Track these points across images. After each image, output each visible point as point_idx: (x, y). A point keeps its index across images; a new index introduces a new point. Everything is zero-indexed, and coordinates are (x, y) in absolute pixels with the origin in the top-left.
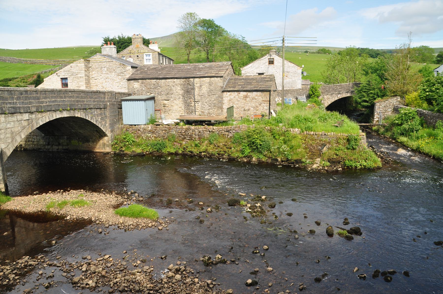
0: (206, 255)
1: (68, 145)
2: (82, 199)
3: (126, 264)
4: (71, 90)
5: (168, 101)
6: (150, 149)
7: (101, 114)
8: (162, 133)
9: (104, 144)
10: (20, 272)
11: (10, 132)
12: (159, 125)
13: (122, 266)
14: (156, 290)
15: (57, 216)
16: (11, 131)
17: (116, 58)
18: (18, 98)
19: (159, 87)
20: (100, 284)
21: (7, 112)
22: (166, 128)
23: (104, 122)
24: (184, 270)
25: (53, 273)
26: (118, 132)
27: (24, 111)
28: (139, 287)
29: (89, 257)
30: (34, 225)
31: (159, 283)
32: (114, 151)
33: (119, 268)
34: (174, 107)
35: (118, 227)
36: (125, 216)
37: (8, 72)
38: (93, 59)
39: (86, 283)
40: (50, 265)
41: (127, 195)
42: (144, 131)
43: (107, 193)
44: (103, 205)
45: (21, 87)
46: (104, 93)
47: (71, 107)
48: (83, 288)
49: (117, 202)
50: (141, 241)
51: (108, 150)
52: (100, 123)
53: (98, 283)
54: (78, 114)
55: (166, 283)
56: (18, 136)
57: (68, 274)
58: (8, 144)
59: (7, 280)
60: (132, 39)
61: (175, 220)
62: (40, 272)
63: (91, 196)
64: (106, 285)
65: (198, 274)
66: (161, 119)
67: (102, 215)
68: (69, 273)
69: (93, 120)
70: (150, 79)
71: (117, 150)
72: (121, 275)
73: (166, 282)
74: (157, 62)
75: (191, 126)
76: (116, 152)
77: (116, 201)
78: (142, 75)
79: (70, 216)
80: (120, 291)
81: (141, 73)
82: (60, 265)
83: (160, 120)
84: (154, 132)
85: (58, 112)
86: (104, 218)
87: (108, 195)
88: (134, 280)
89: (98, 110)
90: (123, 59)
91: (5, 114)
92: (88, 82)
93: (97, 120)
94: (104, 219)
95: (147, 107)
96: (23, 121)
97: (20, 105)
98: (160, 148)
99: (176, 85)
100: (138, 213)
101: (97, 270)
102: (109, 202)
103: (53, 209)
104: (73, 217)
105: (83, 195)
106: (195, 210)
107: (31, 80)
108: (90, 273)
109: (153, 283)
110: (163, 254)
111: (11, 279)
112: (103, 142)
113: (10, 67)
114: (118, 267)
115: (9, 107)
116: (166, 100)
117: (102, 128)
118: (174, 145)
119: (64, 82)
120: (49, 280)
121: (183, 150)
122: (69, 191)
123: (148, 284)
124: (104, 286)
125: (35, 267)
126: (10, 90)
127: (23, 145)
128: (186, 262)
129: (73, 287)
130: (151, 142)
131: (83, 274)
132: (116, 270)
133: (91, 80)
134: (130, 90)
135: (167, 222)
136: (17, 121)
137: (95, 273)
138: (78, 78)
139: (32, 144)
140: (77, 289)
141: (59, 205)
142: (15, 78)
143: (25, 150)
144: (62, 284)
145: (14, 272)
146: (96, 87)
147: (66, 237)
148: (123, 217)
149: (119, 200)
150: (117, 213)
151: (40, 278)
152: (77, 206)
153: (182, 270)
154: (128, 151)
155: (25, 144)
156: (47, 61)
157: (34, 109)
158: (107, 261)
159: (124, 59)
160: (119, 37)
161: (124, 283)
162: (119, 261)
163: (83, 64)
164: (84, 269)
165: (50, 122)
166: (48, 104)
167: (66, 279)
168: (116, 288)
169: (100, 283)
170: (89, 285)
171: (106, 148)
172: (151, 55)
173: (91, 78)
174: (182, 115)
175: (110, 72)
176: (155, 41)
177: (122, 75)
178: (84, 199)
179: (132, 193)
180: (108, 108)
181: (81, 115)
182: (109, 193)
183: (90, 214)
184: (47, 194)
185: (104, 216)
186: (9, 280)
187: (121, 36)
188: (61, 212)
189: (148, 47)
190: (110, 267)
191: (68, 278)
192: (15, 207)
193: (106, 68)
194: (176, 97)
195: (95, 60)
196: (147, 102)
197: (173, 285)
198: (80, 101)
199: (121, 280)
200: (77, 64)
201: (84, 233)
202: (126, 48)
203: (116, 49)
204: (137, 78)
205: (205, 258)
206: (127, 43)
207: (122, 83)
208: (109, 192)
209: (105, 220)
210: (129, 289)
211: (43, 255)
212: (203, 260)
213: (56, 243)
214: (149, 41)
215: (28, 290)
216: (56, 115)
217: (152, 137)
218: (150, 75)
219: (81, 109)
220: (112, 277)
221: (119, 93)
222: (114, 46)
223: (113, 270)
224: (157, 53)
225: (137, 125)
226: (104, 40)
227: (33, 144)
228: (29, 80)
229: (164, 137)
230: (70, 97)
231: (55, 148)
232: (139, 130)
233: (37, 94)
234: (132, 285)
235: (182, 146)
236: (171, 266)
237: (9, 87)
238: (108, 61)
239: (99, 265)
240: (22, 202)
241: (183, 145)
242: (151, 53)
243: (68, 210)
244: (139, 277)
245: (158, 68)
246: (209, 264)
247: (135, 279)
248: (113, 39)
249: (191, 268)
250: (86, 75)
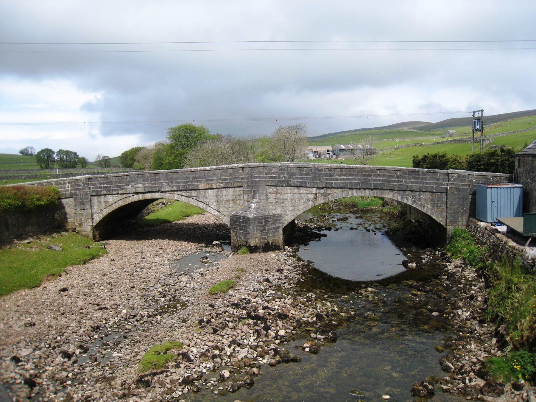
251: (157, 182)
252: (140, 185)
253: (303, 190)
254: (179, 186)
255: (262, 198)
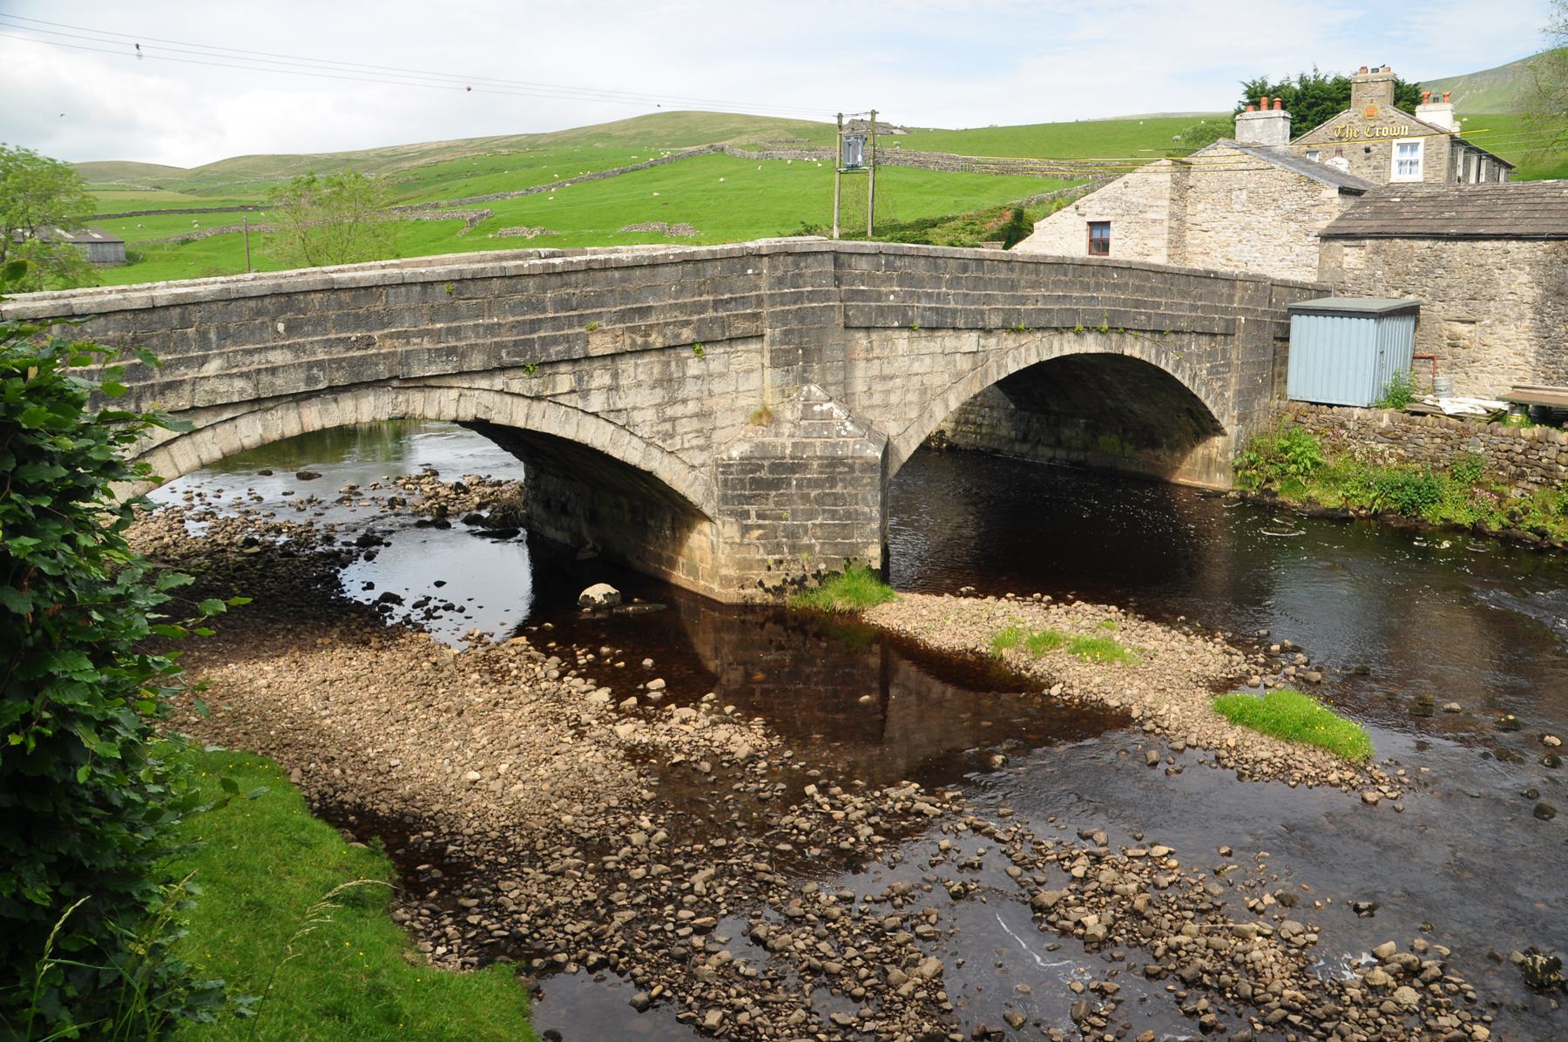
0: (1542, 947)
1: (1085, 449)
2: (1111, 638)
3: (1221, 894)
4: (1121, 262)
5: (1472, 327)
6: (1375, 499)
7: (1211, 355)
8: (1429, 446)
9: (1209, 462)
10: (888, 826)
11: (918, 386)
12: (1424, 414)
13: (1208, 897)
14: (1315, 1017)
15: (1020, 676)
16: (922, 384)
17: (1286, 154)
18: (955, 282)
19: (1440, 271)
20: (1121, 935)
21: (918, 323)
22: (1448, 426)
23: (1220, 383)
24: (1436, 979)
25: (980, 855)
26: (1263, 423)
27: (966, 322)
28: (1254, 987)
29: (1101, 837)
30: (944, 693)
31: (1329, 994)
32: (1239, 488)
33: (1194, 902)
34: (1492, 351)
35: (1218, 759)
36: (1248, 725)
37: (929, 198)
38: (1202, 161)
39: (1076, 919)
40: (976, 829)
41: (1267, 651)
42: (1362, 431)
43: (1197, 633)
44: (1176, 673)
45: (963, 245)
46: (1231, 280)
47: (1113, 322)
48: (1064, 932)
49: (1227, 670)
50: (1291, 828)
51: (1220, 482)
52: (1205, 384)
53: (1116, 930)
54: (1133, 346)
55: (1357, 1004)
56: (938, 401)
57: (1025, 873)
58: (907, 423)
59: (852, 840)
60: (1354, 86)
61: (1435, 780)
62: (945, 843)
63: (1141, 633)
64: (1139, 944)
65: (1494, 1012)
66: (1434, 390)
67: (1167, 706)
68: (1028, 870)
69: (1183, 371)
70: (1409, 238)
71: (1251, 486)
72: (1197, 926)
73: (1355, 998)
74: (1444, 173)
75: (1553, 430)
76: (1246, 493)
77: (1225, 666)
78: (1379, 223)
79: (1061, 685)
80: (1183, 980)
81: (1377, 214)
82: (1007, 839)
83: (1430, 396)
84: (1400, 438)
85: (1071, 336)
86: (1173, 716)
87: (1199, 642)
88: (1240, 957)
89: (1204, 340)
90: (1312, 158)
91: (911, 328)
92: (1177, 240)
93: (1195, 375)
94: (1171, 721)
95: (1383, 343)
96: (958, 356)
97: (956, 303)
98: (1414, 502)
99: (1514, 263)
100: (1298, 724)
101: (1119, 888)
102: (1198, 666)
103: (1012, 651)
104: (1070, 692)
105: (1116, 624)
106: (1521, 761)
107: (994, 225)
108: (1095, 890)
109: (1307, 989)
110: (1366, 896)
111: (862, 839)
112: (1206, 452)
113: (937, 182)
114: (1192, 895)
115: (925, 309)
116: (1463, 322)
117: (1208, 403)
118: (1472, 498)
119: (1097, 234)
120: (966, 876)
121: (1506, 521)
122: (1069, 603)
123: (1286, 987)
124: (1135, 946)
125: (930, 822)
126: (933, 254)
127: (949, 434)
128: (1452, 949)
129: (1034, 919)
130: (1384, 474)
131: (1073, 886)
132: (1182, 903)
133: (1188, 233)
134: (1327, 276)
135: (1400, 782)
136: (943, 353)
137: (1111, 893)
138: (1144, 224)
139: (975, 433)
140: (1046, 929)
141: (1034, 642)
142: (949, 220)
143: (953, 448)
144: (1002, 899)
145: (874, 820)
146: (1204, 257)
147: (1038, 751)
148: (1238, 728)
149: (1234, 663)
150: (1222, 710)
151: (941, 862)
152: (1089, 658)
153: (1427, 975)
154: (1290, 496)
155: (954, 430)
156: (1049, 164)
157: (995, 321)
158: (1157, 865)
159: (1316, 159)
160: (1302, 79)
161: (1204, 957)
162: (1201, 876)
163: (1168, 177)
164: (1078, 872)
165: (1040, 367)
166: (1040, 306)
167: (1016, 886)
168: (1172, 966)
169: (1123, 931)
170: (1085, 927)
171: (1212, 474)
172: (1421, 148)
173: (1188, 225)
174: (1523, 384)
175: (1260, 207)
176: (1442, 91)
177: (1300, 218)
178: (1117, 638)
179: (1284, 649)
180: (1240, 334)
181: (1142, 352)
182: (1203, 636)
183: (1128, 692)
184: (999, 598)
185: (1176, 709)
186: (857, 839)
187: (1310, 75)
188: (1035, 667)
189: (1413, 113)
190: (1164, 888)
191: (1022, 887)
192: (900, 622)
193: (1245, 192)
194: (1508, 312)
195: (1211, 163)
196: (1389, 325)
197: (1382, 1020)
198: (1145, 304)
199: (1194, 943)
200: (1147, 176)
201: (1112, 749)
202: (1325, 119)
203: (1288, 124)
204: (1358, 230)
205: (1534, 960)
206: (1331, 100)
207: (1297, 249)
208: (1204, 631)
209: (1175, 725)
210: (1218, 982)
211: (959, 793)
212: (1522, 964)
213: (1005, 762)
214: (1417, 92)
215: (902, 887)
216: (1062, 345)
217: (1391, 455)
218: (1411, 222)
219: (1144, 331)
220: (1166, 924)
221: (1285, 285)
222: (1282, 113)
223: (1172, 899)
224: (1445, 139)
225: (1339, 406)
226: (1247, 92)
227: (976, 433)
228: (987, 227)
229: (1438, 461)
230: (1116, 287)
231: (1045, 454)
232: (1342, 426)
233: (1012, 270)
234: (1230, 973)
235: (1504, 505)
236: (1388, 947)
237: (931, 247)
238: (1254, 165)
239: (1130, 870)
240: (924, 612)
241: (1509, 501)
242: (1421, 140)
243: (1059, 666)
244: (1261, 953)
245: (1445, 195)
246: (1549, 986)
247: (1245, 953)
248: (1282, 87)
249: (1468, 980)
250: (1172, 215)
251: (376, 334)
252: (277, 358)
253: (949, 341)
254: (500, 346)
255: (830, 379)
